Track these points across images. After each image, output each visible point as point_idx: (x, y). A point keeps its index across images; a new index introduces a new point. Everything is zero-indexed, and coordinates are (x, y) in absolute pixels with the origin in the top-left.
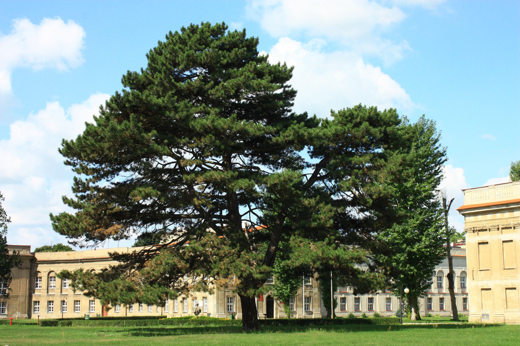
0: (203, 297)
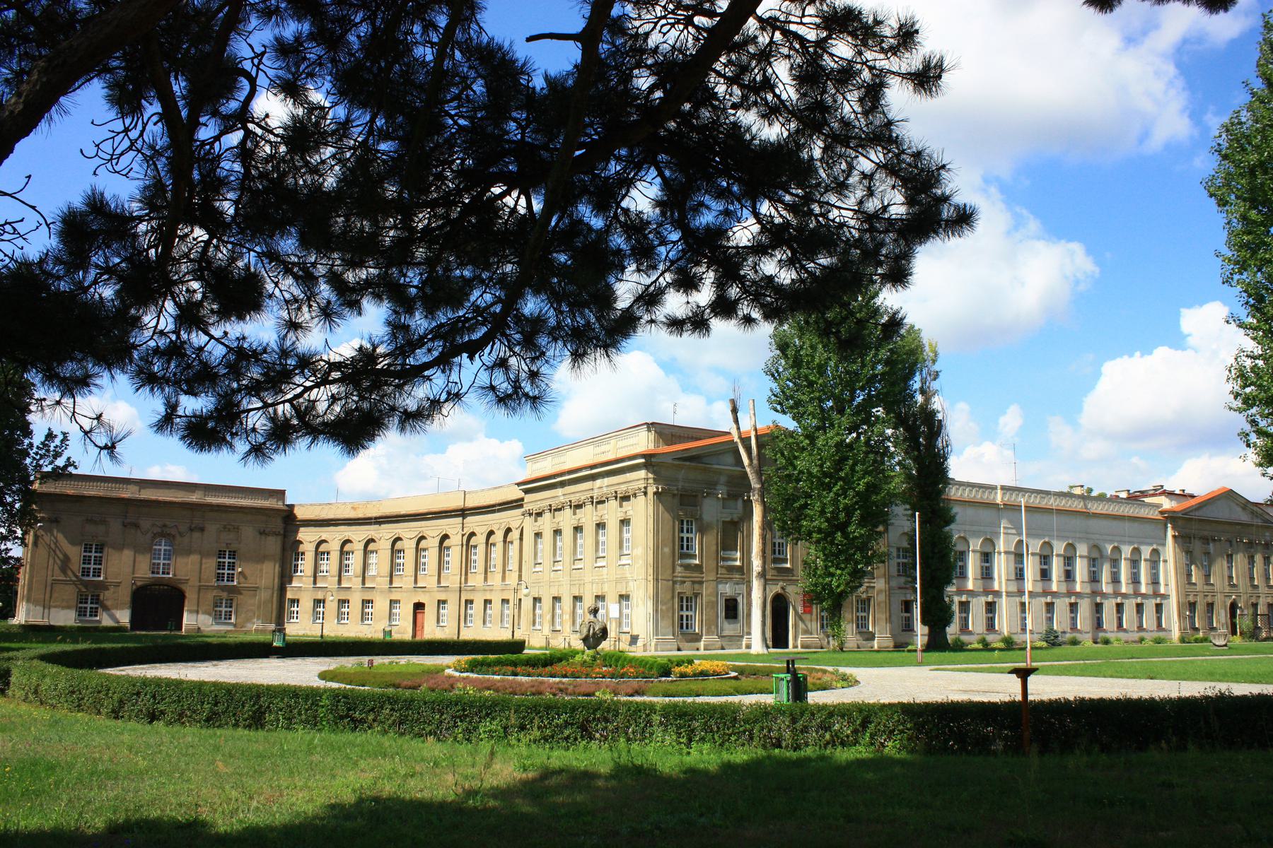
0: (621, 596)
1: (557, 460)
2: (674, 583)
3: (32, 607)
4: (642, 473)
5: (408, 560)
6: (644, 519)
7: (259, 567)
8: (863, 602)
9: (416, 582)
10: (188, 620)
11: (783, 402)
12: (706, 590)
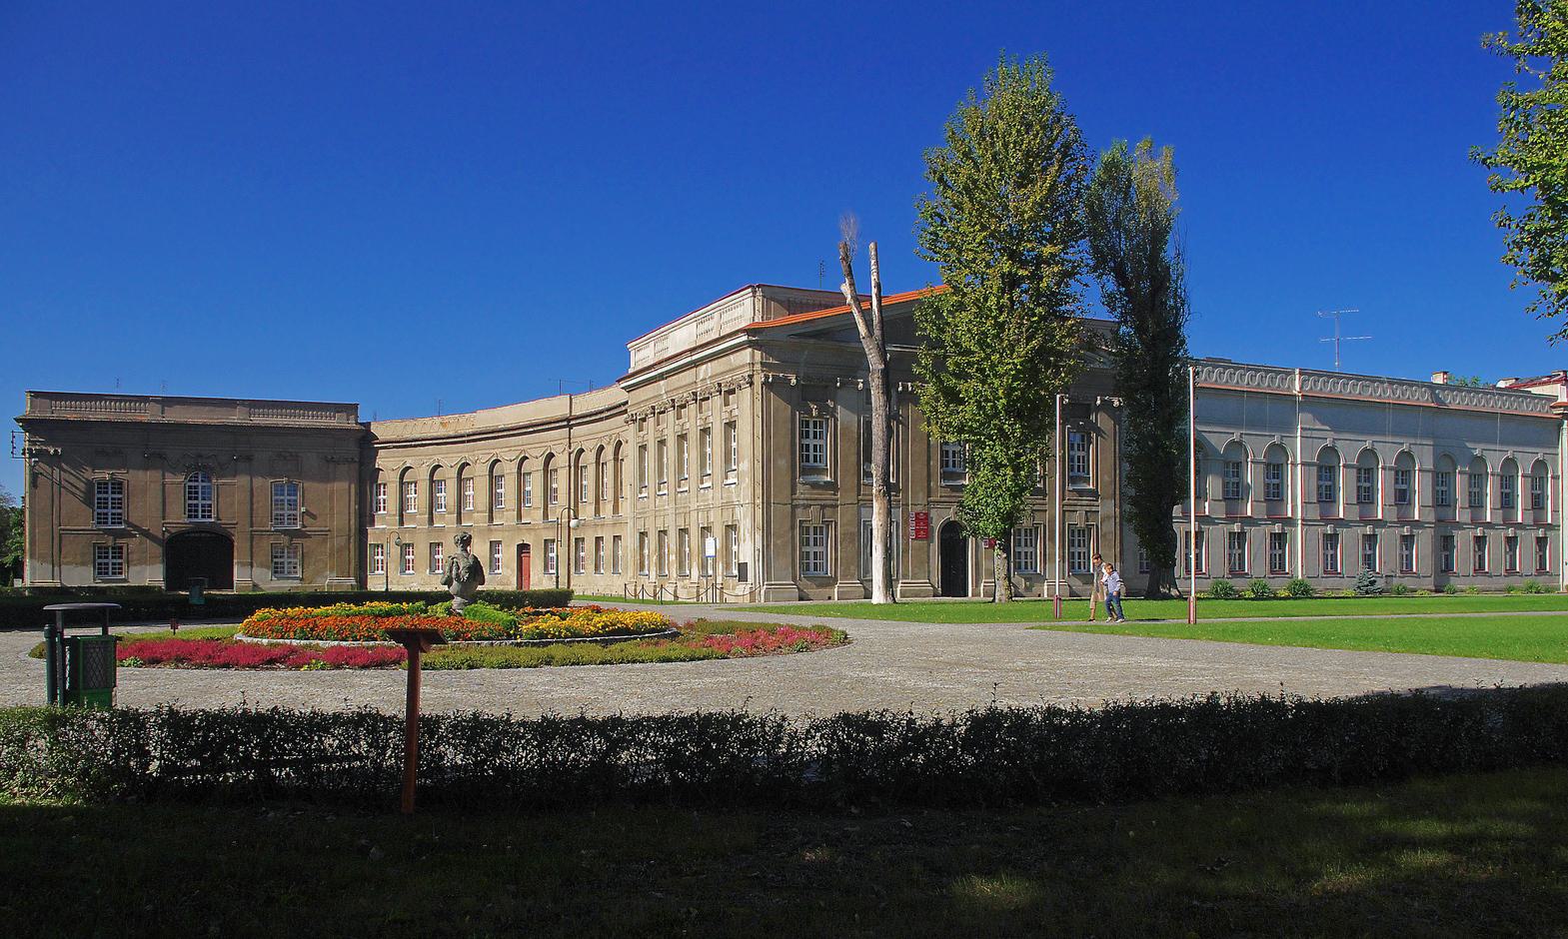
2: (794, 507)
3: (38, 564)
4: (746, 355)
5: (508, 490)
9: (519, 517)
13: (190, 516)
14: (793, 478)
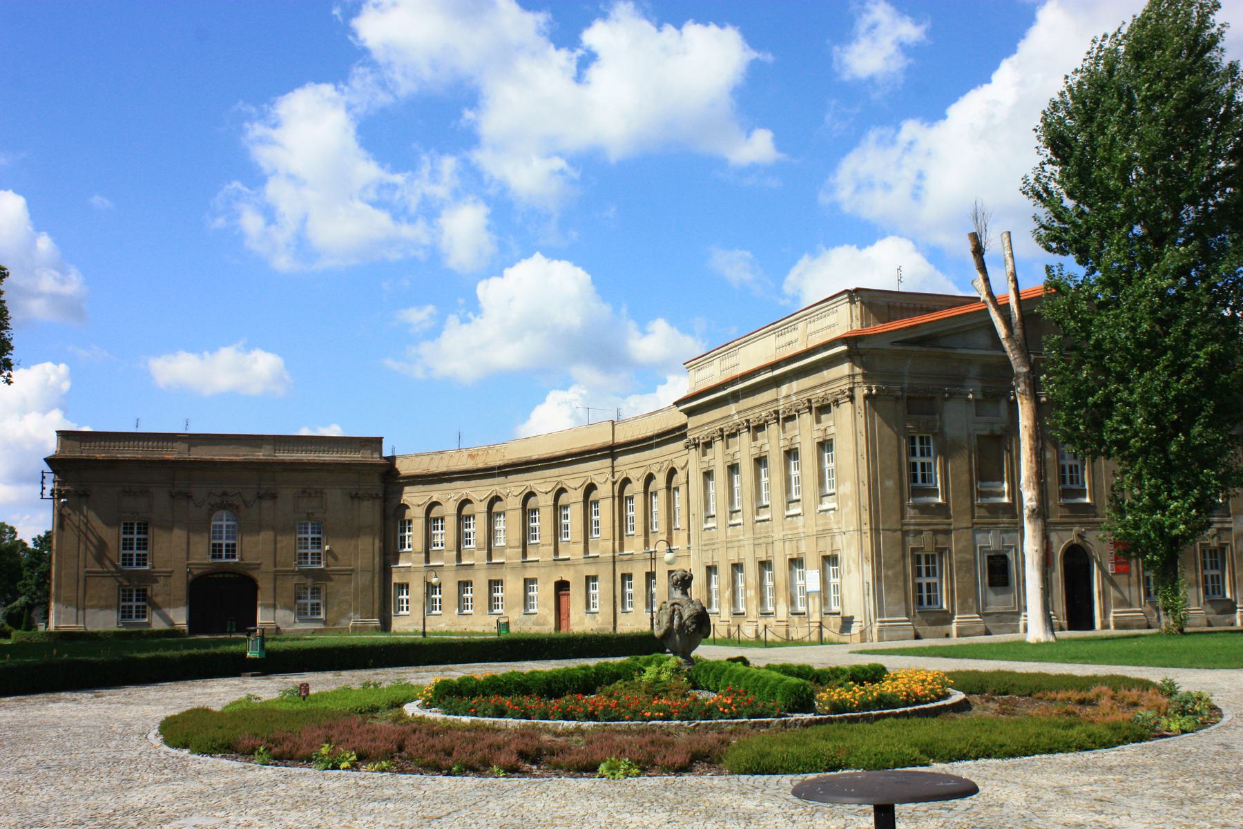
1: (728, 362)
2: (905, 533)
3: (62, 608)
4: (845, 369)
5: (543, 523)
6: (851, 438)
7: (353, 542)
8: (1214, 552)
9: (556, 552)
10: (263, 617)
11: (1057, 238)
12: (956, 544)
13: (214, 557)
14: (902, 501)
